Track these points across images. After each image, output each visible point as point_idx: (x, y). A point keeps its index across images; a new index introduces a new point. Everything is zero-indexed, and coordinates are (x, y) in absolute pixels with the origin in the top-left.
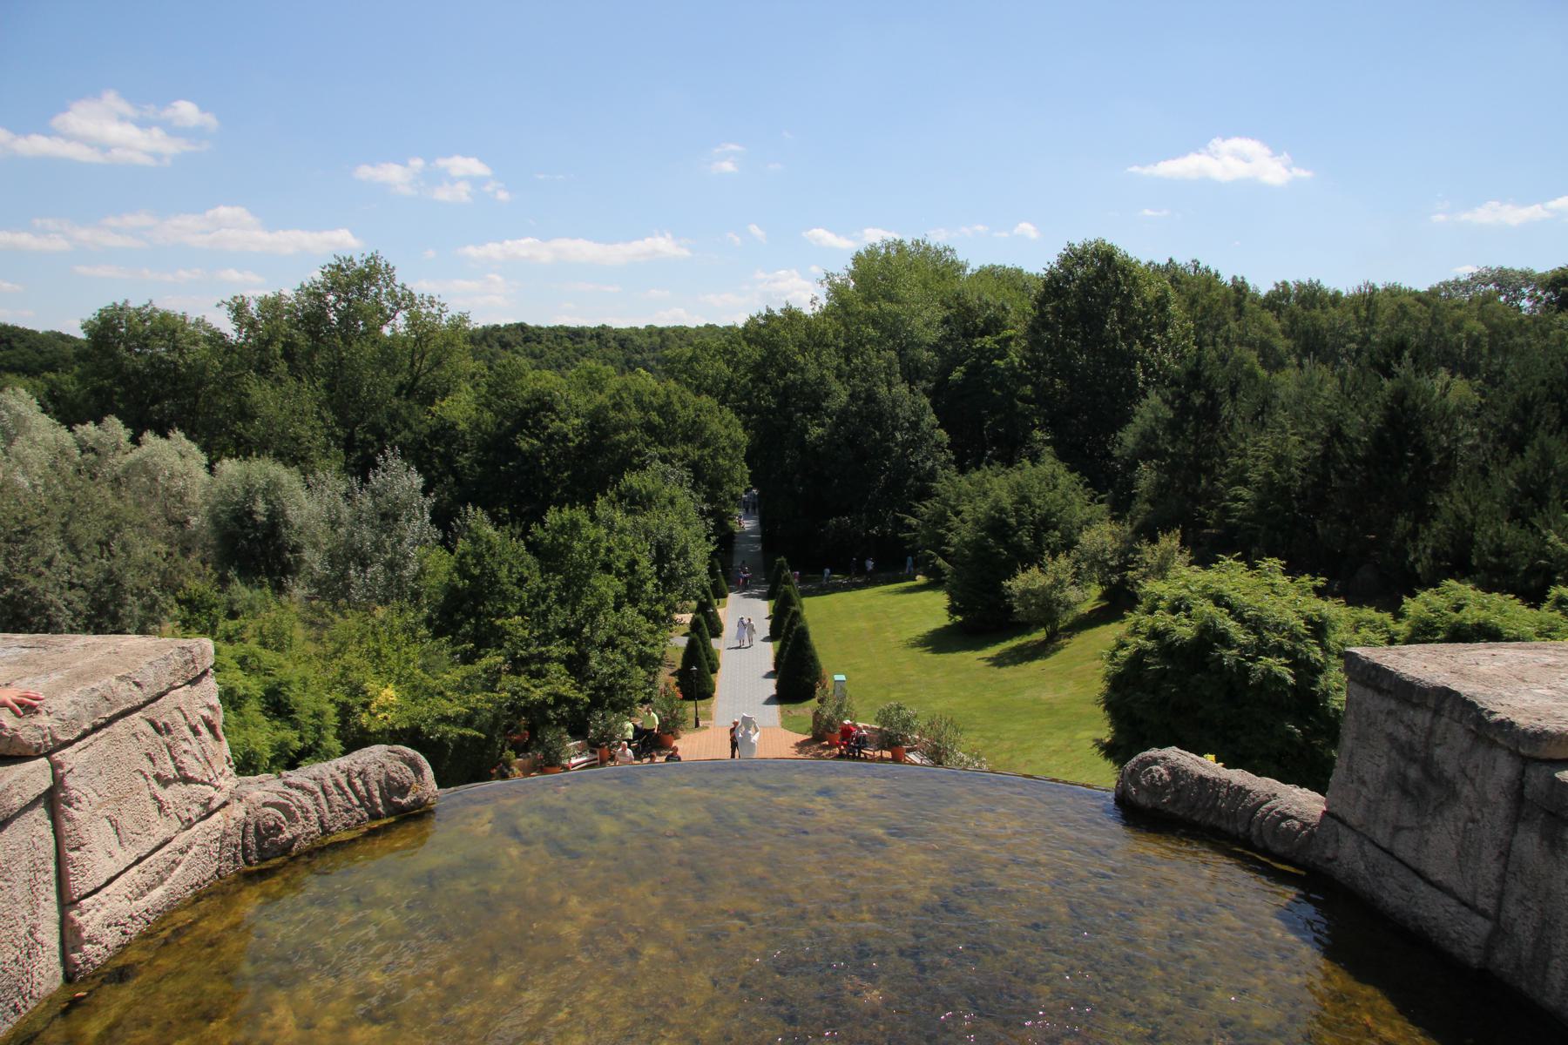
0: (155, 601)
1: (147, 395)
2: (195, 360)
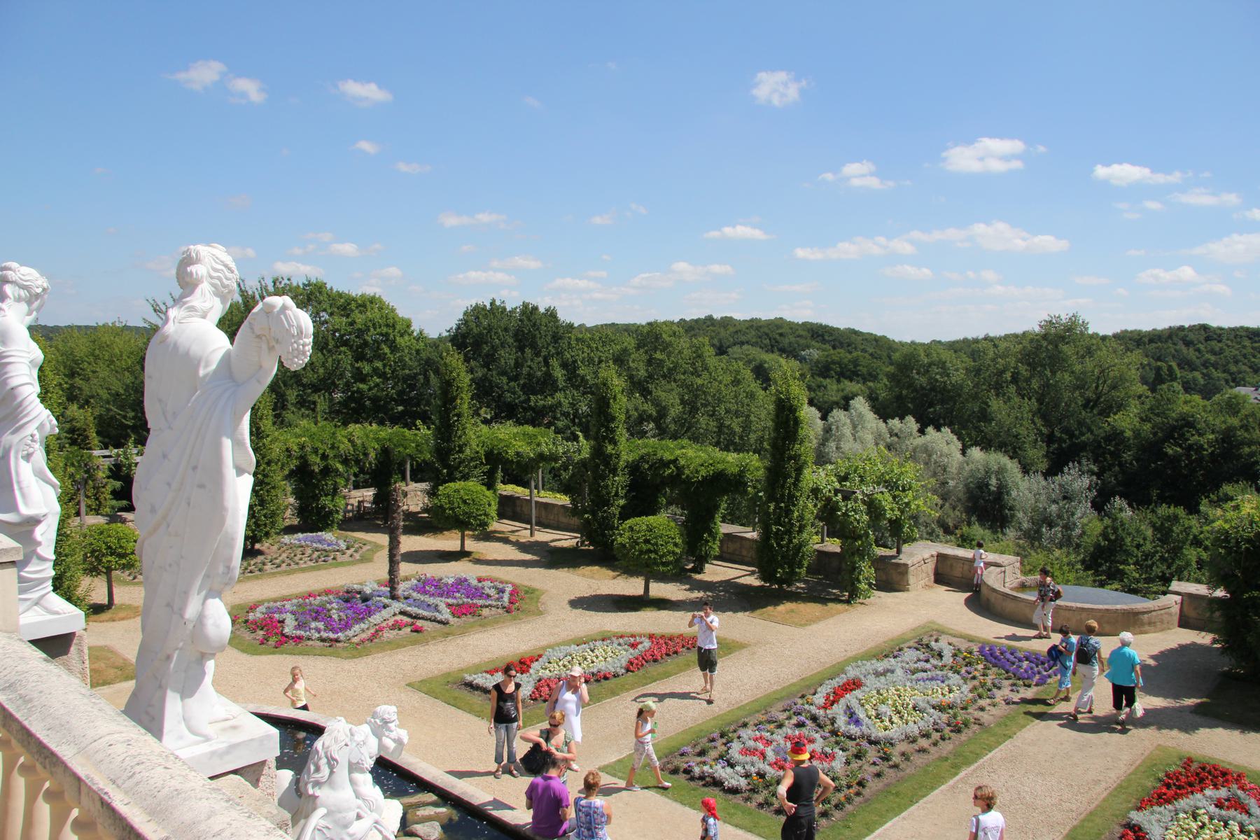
0: (933, 531)
1: (926, 401)
2: (956, 382)
